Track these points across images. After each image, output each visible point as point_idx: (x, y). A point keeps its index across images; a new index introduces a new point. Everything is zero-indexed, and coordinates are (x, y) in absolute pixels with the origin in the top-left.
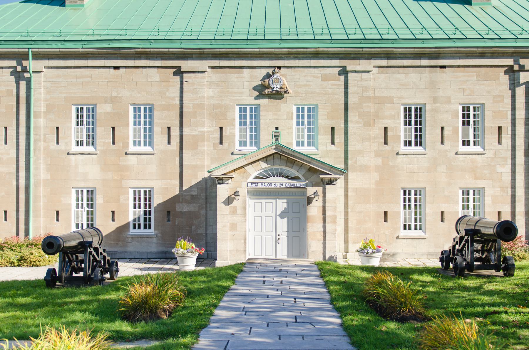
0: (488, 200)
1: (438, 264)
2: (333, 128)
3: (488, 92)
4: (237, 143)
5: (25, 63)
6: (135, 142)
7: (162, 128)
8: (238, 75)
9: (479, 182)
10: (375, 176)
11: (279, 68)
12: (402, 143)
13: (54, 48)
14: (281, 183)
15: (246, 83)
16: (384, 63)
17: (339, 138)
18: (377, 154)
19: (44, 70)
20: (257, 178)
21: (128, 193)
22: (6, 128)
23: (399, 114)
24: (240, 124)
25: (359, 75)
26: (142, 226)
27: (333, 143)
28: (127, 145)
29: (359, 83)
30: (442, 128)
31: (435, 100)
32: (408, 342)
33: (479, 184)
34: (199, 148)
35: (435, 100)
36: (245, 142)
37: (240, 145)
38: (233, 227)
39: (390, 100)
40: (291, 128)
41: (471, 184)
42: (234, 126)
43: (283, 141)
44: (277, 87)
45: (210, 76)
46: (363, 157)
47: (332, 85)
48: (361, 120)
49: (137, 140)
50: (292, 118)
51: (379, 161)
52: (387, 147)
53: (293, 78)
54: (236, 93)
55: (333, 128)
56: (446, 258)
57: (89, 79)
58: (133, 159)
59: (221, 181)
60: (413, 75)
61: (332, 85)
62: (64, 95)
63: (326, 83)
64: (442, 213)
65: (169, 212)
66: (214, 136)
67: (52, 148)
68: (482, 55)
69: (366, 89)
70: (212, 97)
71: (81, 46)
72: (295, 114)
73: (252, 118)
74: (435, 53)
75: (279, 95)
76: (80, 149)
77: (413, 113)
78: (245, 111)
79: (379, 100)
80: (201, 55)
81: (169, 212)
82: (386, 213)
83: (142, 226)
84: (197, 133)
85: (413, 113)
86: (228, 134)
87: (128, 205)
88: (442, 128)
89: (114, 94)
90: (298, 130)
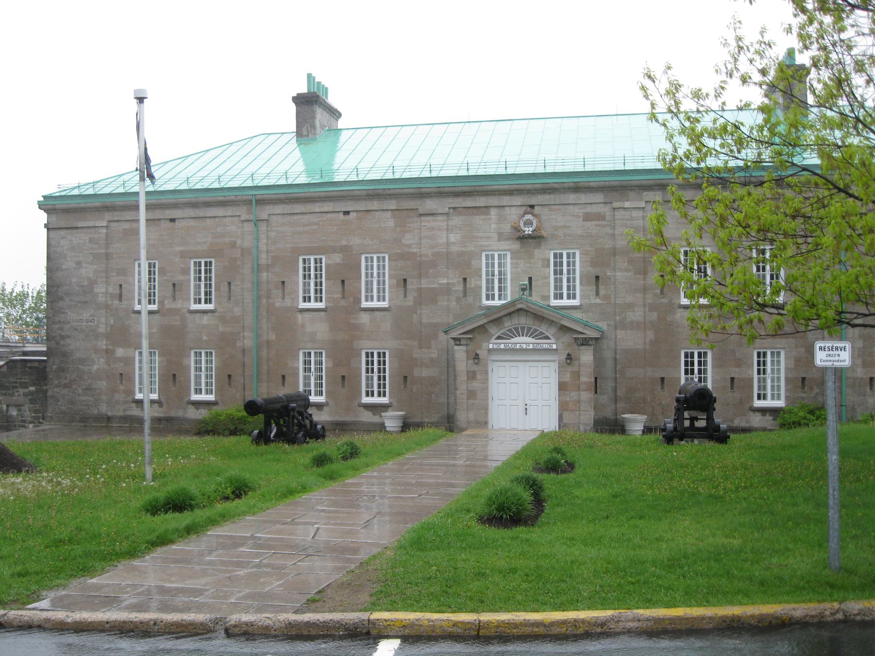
4: (301, 299)
6: (304, 298)
7: (397, 281)
8: (483, 217)
12: (192, 300)
15: (493, 226)
26: (376, 393)
29: (628, 222)
32: (686, 557)
34: (439, 303)
36: (200, 300)
40: (548, 277)
42: (481, 276)
46: (634, 311)
47: (597, 225)
48: (631, 267)
49: (490, 293)
50: (549, 266)
54: (481, 238)
57: (316, 227)
58: (365, 318)
61: (597, 225)
62: (289, 246)
63: (589, 224)
65: (405, 378)
66: (456, 288)
71: (221, 194)
77: (203, 268)
81: (405, 378)
83: (376, 393)
84: (436, 286)
85: (203, 268)
86: (473, 286)
89: (344, 243)
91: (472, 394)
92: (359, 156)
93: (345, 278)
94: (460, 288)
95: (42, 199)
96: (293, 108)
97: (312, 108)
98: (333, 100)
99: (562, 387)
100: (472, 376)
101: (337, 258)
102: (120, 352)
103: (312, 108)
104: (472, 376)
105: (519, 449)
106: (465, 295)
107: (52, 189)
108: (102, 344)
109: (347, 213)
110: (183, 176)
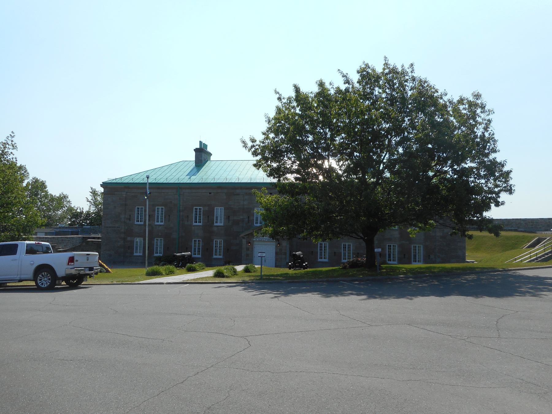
91: (247, 255)
92: (211, 174)
93: (209, 215)
94: (247, 220)
95: (505, 169)
96: (194, 153)
97: (202, 155)
98: (209, 150)
99: (276, 253)
100: (248, 249)
101: (207, 208)
102: (129, 239)
103: (202, 155)
104: (248, 249)
105: (54, 189)
106: (248, 222)
107: (105, 180)
108: (122, 236)
109: (210, 193)
110: (165, 177)
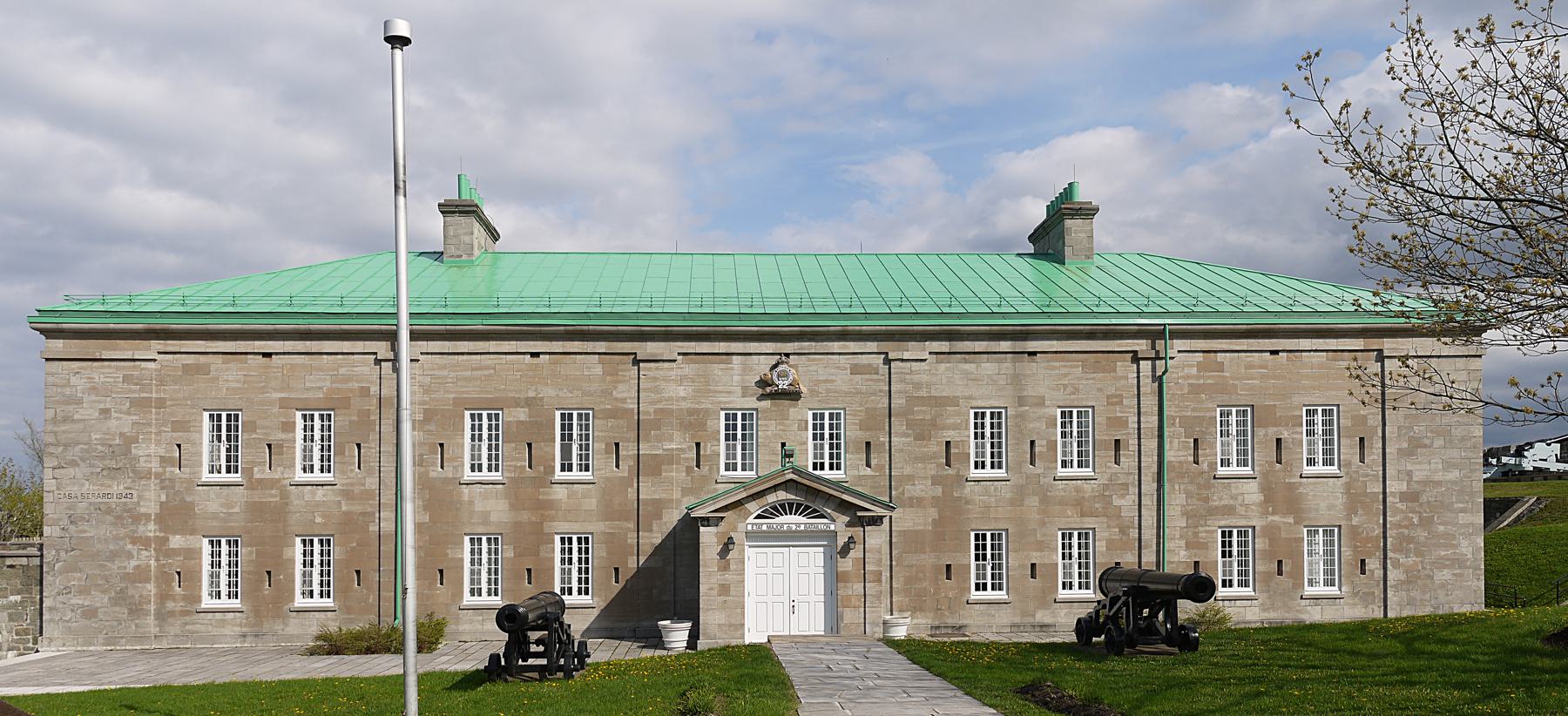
0: (1101, 546)
1: (1073, 638)
2: (868, 444)
3: (1100, 390)
4: (722, 467)
5: (1160, 344)
9: (1087, 519)
10: (933, 513)
11: (787, 355)
13: (139, 324)
14: (798, 525)
16: (944, 346)
17: (1374, 455)
18: (936, 481)
19: (421, 357)
20: (758, 517)
21: (553, 542)
22: (530, 445)
23: (967, 421)
24: (727, 438)
25: (908, 364)
27: (868, 465)
28: (1213, 466)
30: (1032, 442)
31: (1021, 401)
33: (1089, 522)
35: (1021, 401)
37: (727, 469)
38: (724, 589)
39: (954, 401)
40: (806, 443)
41: (1075, 521)
43: (797, 461)
44: (783, 384)
45: (688, 368)
51: (939, 491)
52: (950, 471)
53: (809, 370)
55: (868, 444)
56: (1085, 628)
59: (706, 521)
60: (988, 367)
64: (1033, 565)
67: (432, 474)
68: (1091, 334)
69: (918, 386)
70: (684, 399)
72: (1059, 420)
73: (739, 428)
74: (1021, 332)
75: (793, 395)
76: (477, 476)
78: (822, 418)
79: (941, 402)
80: (668, 336)
82: (949, 567)
87: (553, 559)
88: (1032, 442)
89: (532, 394)
90: (728, 447)
